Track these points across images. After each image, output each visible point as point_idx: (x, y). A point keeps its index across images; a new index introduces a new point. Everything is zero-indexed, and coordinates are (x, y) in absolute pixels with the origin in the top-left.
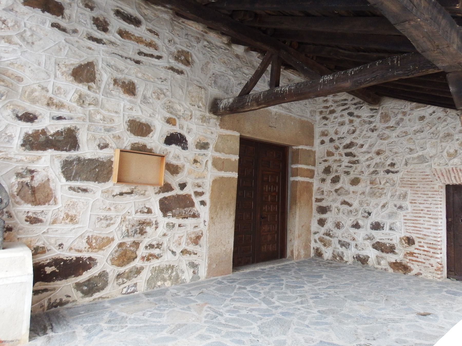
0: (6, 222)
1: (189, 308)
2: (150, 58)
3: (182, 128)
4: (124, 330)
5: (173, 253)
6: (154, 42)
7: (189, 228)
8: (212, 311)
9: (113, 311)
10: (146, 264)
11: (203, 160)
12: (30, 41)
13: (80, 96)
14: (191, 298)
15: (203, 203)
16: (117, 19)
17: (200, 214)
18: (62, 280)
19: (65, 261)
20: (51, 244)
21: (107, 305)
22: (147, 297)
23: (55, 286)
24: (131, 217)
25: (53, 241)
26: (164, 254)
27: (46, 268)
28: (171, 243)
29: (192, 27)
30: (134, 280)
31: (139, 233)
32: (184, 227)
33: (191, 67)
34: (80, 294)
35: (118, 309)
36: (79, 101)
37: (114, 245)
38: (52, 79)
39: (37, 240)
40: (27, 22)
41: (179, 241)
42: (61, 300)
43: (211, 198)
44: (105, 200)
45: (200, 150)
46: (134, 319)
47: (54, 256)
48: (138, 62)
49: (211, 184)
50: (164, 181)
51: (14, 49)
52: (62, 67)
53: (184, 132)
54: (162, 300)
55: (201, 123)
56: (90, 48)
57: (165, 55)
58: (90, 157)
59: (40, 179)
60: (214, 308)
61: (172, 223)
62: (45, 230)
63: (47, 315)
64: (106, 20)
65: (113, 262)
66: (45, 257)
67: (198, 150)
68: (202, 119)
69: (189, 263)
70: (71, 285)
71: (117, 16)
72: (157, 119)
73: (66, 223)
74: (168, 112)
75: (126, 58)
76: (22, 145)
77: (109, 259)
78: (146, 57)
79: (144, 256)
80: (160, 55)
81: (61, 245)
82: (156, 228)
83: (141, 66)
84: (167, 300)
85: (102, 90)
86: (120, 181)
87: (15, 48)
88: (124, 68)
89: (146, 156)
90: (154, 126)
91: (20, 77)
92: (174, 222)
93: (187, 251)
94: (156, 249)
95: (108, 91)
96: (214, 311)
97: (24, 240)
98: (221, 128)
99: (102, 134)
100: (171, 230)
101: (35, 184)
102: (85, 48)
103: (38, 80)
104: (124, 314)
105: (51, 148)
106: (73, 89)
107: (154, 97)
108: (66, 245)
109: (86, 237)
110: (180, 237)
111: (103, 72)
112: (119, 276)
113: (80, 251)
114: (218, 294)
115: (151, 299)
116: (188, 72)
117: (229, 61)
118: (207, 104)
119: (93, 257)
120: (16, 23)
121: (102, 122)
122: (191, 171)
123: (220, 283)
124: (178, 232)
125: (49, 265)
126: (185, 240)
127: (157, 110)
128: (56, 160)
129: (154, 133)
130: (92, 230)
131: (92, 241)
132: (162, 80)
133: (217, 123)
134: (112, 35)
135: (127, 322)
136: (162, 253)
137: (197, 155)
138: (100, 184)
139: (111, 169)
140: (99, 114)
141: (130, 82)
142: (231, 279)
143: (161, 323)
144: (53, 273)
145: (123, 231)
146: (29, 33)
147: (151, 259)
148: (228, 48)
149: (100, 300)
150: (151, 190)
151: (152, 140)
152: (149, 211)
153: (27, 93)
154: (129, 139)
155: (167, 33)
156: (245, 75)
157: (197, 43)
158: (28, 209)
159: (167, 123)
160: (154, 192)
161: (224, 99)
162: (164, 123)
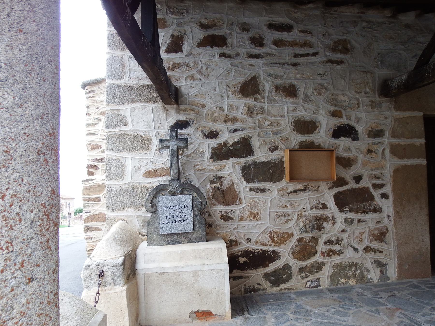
0: (206, 220)
1: (377, 311)
2: (306, 57)
3: (349, 118)
4: (308, 323)
5: (356, 250)
6: (308, 40)
7: (371, 224)
8: (406, 319)
9: (298, 303)
10: (327, 259)
11: (378, 149)
12: (206, 74)
13: (249, 108)
14: (380, 300)
15: (384, 196)
16: (270, 32)
17: (382, 208)
18: (253, 269)
19: (253, 253)
20: (241, 238)
21: (293, 296)
22: (331, 293)
23: (248, 274)
24: (307, 213)
25: (242, 236)
26: (345, 250)
27: (239, 258)
28: (352, 239)
29: (346, 12)
30: (317, 275)
31: (317, 229)
32: (365, 223)
33: (351, 53)
34: (269, 284)
35: (302, 301)
36: (249, 113)
37: (294, 240)
38: (226, 100)
39: (230, 234)
40: (202, 59)
41: (361, 237)
42: (254, 287)
43: (394, 190)
44: (281, 198)
45: (373, 139)
46: (319, 314)
47: (244, 248)
48: (295, 65)
49: (392, 174)
50: (337, 175)
51: (196, 84)
52: (231, 88)
53: (353, 123)
54: (347, 298)
55: (371, 110)
56: (251, 65)
57: (321, 50)
58: (263, 161)
59: (227, 184)
60: (409, 316)
61: (350, 218)
62: (235, 226)
63: (244, 298)
64: (261, 36)
65: (295, 256)
66: (238, 249)
67: (371, 139)
68: (371, 106)
69: (375, 261)
70: (261, 274)
71: (270, 29)
72: (321, 114)
73: (251, 220)
74: (332, 105)
75: (284, 64)
76: (211, 158)
77: (290, 253)
78: (302, 58)
79: (324, 251)
80: (316, 52)
81: (249, 239)
82: (334, 223)
83: (299, 68)
84: (352, 299)
85: (266, 99)
86: (292, 179)
87: (196, 83)
88: (282, 74)
89: (315, 152)
90: (319, 122)
91: (203, 104)
92: (352, 217)
93: (371, 248)
94: (335, 245)
95: (271, 98)
96: (409, 318)
97: (221, 235)
98: (397, 111)
99: (272, 138)
100: (350, 226)
101: (224, 188)
102: (248, 66)
103: (215, 103)
104: (309, 308)
105: (232, 157)
106: (242, 104)
107: (316, 94)
108: (253, 239)
109: (268, 233)
110: (362, 234)
111: (265, 83)
112: (302, 270)
113: (265, 245)
114: (413, 300)
115: (336, 296)
116: (348, 60)
117: (397, 35)
118: (375, 88)
119: (276, 251)
120: (195, 63)
121: (269, 127)
122: (366, 162)
123: (416, 287)
124: (358, 229)
125: (242, 256)
126: (367, 236)
127: (321, 106)
128: (236, 166)
129: (320, 129)
130: (273, 226)
131: (274, 236)
132: (322, 75)
133: (390, 106)
134: (269, 48)
135: (311, 316)
136: (343, 249)
137: (370, 144)
138: (275, 184)
139: (283, 169)
140: (267, 121)
141: (290, 85)
142: (430, 284)
143: (346, 323)
144: (245, 262)
145: (301, 226)
146: (204, 68)
147: (331, 255)
148: (393, 20)
149: (287, 291)
150: (324, 186)
151: (319, 136)
152: (325, 207)
153: (209, 115)
154: (296, 138)
155: (320, 28)
156: (421, 45)
157: (355, 27)
158: (221, 209)
159: (333, 116)
160: (327, 188)
161: (396, 77)
162: (329, 117)
